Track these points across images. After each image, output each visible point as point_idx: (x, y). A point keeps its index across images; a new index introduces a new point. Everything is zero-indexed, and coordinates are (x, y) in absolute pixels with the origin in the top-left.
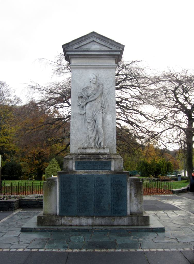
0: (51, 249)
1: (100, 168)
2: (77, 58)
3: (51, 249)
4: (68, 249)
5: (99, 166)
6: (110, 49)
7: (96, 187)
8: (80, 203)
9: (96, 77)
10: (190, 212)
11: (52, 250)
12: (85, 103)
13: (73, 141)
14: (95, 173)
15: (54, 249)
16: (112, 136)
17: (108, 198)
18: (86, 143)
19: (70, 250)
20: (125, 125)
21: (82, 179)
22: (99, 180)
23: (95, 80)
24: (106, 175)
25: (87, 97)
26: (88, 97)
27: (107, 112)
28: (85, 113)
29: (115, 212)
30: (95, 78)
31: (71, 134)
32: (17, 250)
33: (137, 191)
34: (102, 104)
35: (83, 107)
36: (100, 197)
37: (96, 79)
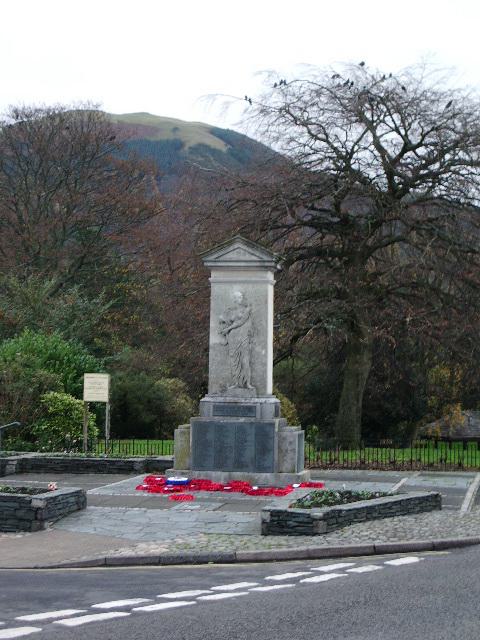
14: (233, 420)
17: (250, 452)
21: (220, 428)
22: (241, 428)
26: (232, 322)
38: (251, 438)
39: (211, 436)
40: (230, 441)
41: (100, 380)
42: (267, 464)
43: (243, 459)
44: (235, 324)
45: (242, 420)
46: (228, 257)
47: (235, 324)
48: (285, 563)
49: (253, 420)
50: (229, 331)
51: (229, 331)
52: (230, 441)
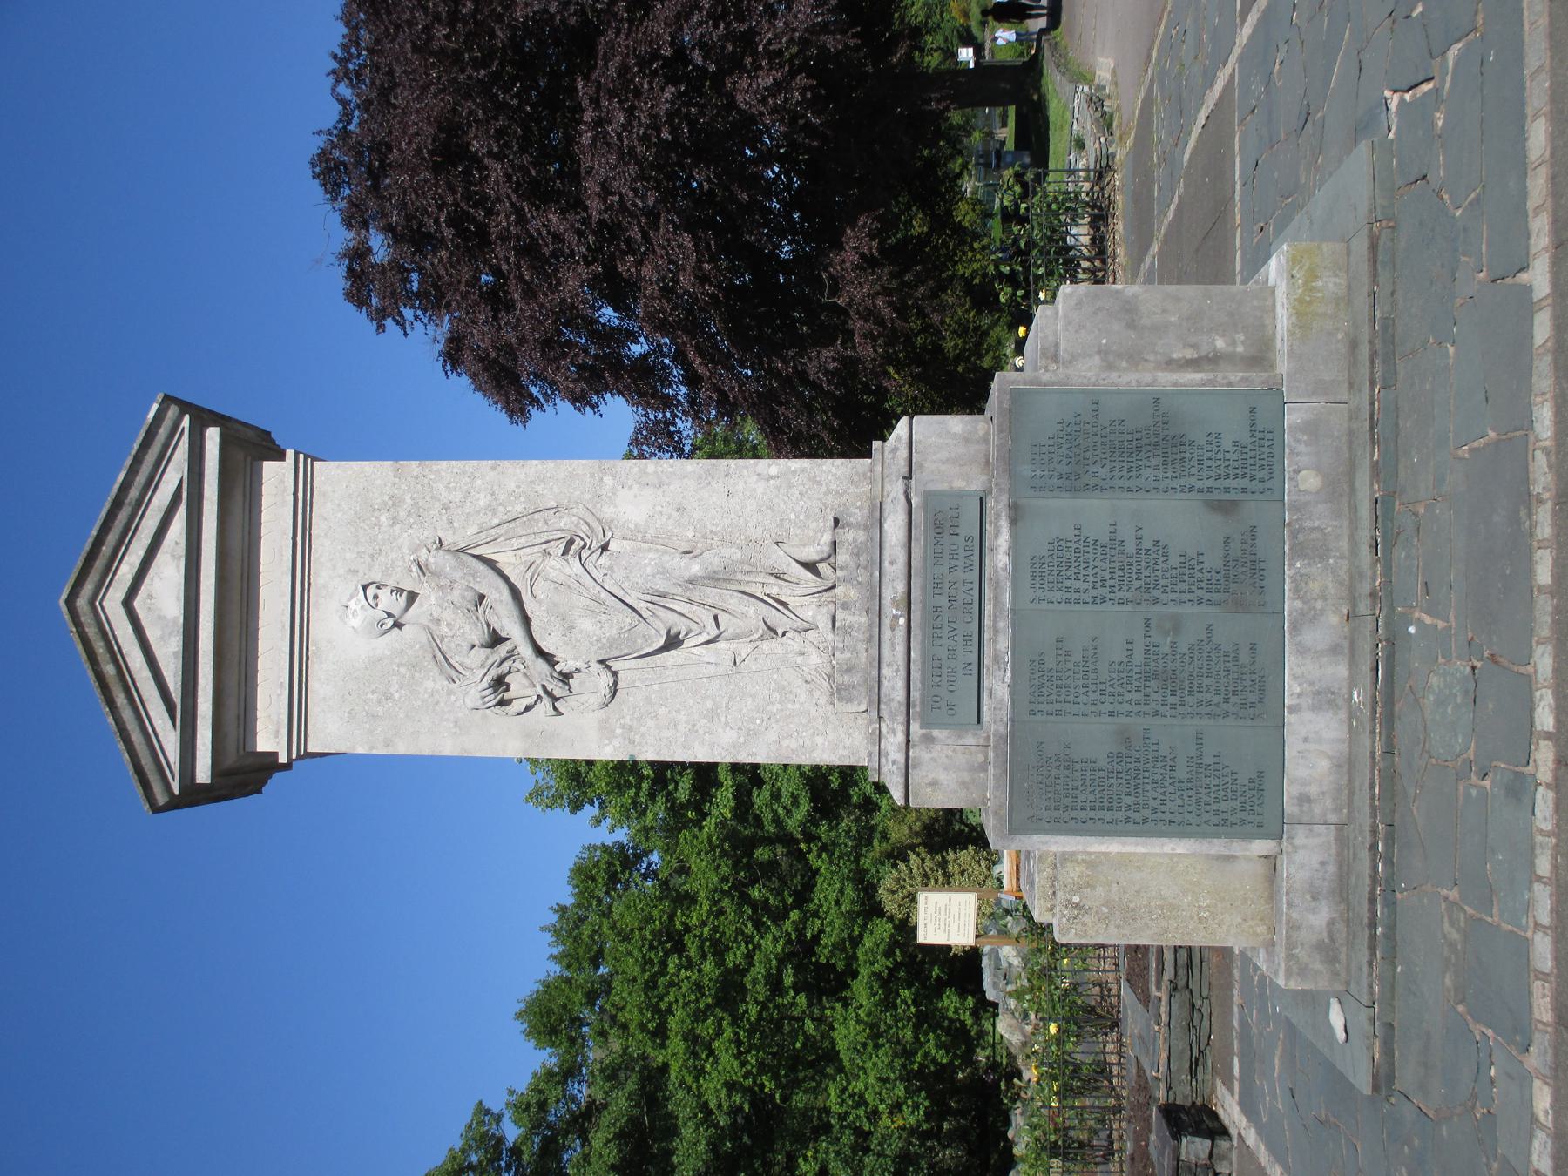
0: (1537, 887)
1: (968, 568)
2: (117, 504)
3: (1530, 889)
4: (1536, 767)
5: (953, 569)
6: (182, 512)
7: (1094, 593)
8: (1200, 704)
9: (365, 587)
10: (1243, 20)
11: (1539, 879)
12: (541, 665)
13: (785, 743)
14: (1001, 600)
15: (1532, 865)
16: (760, 487)
17: (1174, 519)
18: (799, 660)
19: (1544, 758)
20: (570, 862)
21: (1041, 681)
22: (1048, 570)
23: (384, 595)
24: (1014, 522)
25: (503, 649)
26: (495, 640)
27: (600, 521)
28: (602, 662)
29: (1262, 468)
30: (376, 597)
31: (744, 758)
32: (1543, 1127)
33: (802, 774)
34: (546, 553)
35: (565, 677)
36: (1162, 566)
37: (379, 592)
38: (1095, 513)
39: (1092, 736)
40: (1113, 628)
41: (931, 909)
42: (1233, 429)
43: (1214, 560)
44: (510, 627)
45: (1000, 557)
46: (169, 653)
47: (510, 627)
48: (145, 623)
49: (998, 506)
50: (540, 652)
51: (540, 652)
52: (1113, 628)
